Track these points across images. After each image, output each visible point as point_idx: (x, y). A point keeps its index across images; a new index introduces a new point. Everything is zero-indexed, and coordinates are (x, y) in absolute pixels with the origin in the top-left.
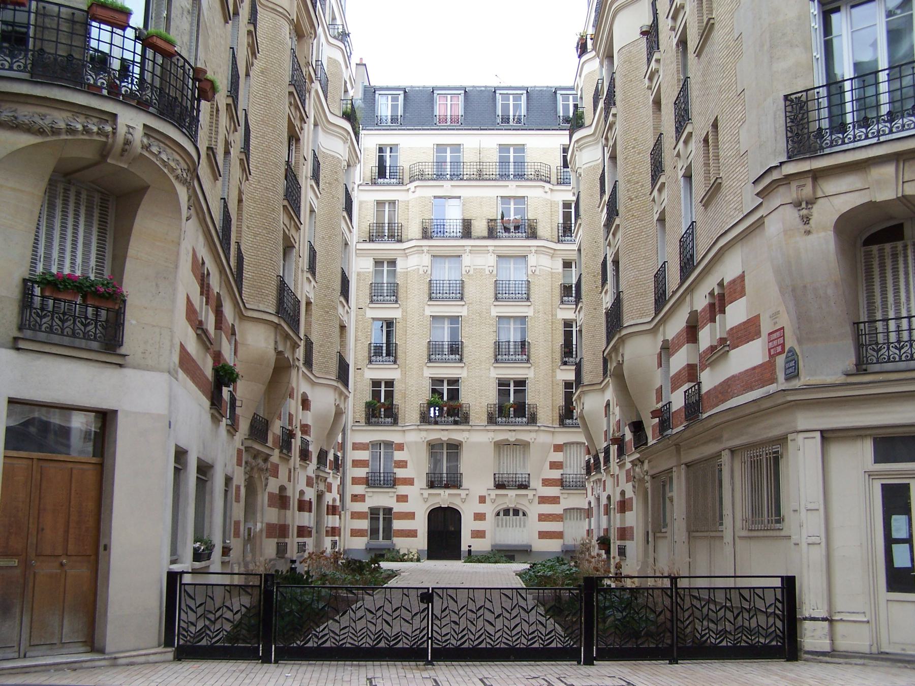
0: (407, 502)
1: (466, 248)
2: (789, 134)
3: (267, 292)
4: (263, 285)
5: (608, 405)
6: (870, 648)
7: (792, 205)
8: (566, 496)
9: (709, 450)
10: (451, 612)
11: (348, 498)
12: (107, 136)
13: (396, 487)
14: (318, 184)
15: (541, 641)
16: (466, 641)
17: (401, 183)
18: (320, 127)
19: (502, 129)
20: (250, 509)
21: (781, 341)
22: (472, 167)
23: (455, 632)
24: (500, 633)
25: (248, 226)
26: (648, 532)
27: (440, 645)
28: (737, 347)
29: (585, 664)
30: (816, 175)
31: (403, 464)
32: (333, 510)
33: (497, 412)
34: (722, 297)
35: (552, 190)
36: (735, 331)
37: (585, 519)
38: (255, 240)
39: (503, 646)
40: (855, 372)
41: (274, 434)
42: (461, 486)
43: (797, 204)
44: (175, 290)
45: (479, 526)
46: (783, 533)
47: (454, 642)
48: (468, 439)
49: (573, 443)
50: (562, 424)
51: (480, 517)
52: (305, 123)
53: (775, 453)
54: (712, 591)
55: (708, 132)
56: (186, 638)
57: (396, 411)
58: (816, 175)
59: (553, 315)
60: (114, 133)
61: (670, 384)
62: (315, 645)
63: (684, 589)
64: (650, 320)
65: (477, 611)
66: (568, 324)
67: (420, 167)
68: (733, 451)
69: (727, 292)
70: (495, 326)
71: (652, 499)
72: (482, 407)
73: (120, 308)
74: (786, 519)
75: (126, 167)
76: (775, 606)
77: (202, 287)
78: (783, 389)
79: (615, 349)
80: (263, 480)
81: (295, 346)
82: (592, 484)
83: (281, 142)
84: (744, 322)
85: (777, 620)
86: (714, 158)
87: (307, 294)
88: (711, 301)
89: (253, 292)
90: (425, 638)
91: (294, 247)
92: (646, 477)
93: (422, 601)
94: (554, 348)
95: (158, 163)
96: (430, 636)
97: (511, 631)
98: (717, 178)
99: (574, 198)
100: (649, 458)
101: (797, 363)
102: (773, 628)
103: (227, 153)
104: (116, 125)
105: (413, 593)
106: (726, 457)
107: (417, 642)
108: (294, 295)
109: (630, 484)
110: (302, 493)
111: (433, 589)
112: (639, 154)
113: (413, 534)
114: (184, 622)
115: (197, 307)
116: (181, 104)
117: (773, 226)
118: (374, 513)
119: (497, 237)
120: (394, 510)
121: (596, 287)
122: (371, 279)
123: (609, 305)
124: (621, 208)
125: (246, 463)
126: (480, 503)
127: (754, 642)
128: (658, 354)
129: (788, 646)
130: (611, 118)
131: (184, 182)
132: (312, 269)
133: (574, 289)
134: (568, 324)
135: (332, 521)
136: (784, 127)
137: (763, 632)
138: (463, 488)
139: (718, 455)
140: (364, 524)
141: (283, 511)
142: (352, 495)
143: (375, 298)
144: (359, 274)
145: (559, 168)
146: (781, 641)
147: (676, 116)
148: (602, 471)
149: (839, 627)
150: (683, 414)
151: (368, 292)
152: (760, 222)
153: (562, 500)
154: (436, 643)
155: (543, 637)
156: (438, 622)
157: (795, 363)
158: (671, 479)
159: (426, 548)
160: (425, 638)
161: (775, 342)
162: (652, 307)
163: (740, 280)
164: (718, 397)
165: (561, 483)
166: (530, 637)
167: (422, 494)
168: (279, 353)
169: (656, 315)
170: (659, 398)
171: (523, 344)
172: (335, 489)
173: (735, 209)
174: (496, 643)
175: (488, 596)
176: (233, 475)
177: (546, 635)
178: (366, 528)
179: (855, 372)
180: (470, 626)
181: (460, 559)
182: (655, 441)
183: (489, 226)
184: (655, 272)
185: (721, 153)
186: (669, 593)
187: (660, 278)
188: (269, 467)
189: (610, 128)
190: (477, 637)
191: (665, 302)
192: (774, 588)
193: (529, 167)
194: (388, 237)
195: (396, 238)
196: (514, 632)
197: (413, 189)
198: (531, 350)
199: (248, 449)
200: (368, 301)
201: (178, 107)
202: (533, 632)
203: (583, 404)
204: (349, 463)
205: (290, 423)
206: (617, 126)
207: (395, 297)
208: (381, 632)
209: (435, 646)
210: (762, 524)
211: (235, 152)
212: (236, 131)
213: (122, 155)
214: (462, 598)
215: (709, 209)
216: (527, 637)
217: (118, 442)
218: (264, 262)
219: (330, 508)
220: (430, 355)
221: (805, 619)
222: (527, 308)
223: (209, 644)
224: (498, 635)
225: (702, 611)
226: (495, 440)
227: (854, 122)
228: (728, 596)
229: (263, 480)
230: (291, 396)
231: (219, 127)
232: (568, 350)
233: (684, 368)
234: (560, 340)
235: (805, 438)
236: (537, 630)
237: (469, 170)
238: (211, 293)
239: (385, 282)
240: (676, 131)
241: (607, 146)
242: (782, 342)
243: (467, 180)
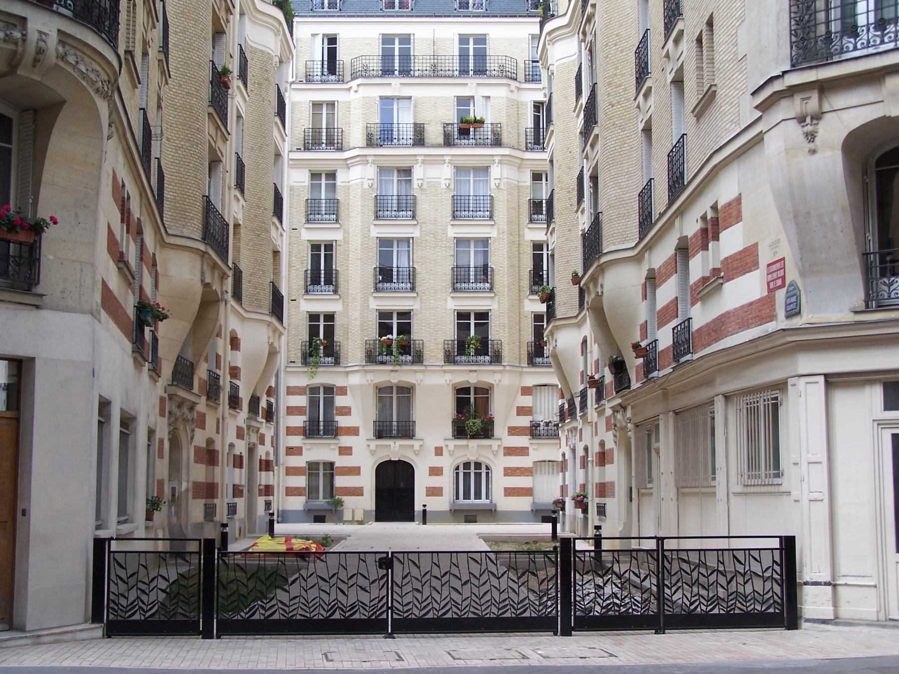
2: (794, 39)
3: (191, 215)
4: (187, 207)
5: (585, 342)
6: (878, 616)
7: (795, 121)
9: (701, 395)
10: (413, 579)
11: (282, 451)
12: (16, 44)
13: (339, 437)
14: (245, 84)
17: (341, 81)
18: (246, 17)
19: (460, 16)
20: (175, 466)
21: (781, 273)
22: (424, 61)
23: (418, 601)
25: (167, 138)
26: (631, 488)
27: (401, 615)
28: (733, 279)
29: (563, 634)
30: (824, 88)
31: (346, 411)
32: (267, 466)
33: (456, 350)
34: (716, 222)
35: (519, 89)
37: (558, 473)
38: (176, 155)
39: (471, 615)
40: (863, 308)
41: (200, 379)
42: (413, 435)
43: (801, 120)
44: (96, 220)
45: (435, 482)
46: (782, 489)
47: (416, 612)
50: (531, 363)
51: (436, 471)
52: (232, 14)
53: (773, 399)
55: (702, 31)
56: (117, 612)
57: (338, 348)
58: (824, 88)
60: (24, 41)
61: (656, 320)
62: (262, 617)
64: (633, 245)
65: (442, 577)
66: (538, 247)
67: (364, 61)
68: (727, 397)
69: (721, 216)
70: (452, 249)
71: (635, 451)
72: (437, 344)
73: (35, 241)
74: (785, 473)
75: (39, 79)
76: (773, 569)
77: (122, 214)
78: (783, 328)
79: (594, 279)
80: (189, 432)
81: (223, 277)
82: (566, 433)
83: (205, 39)
85: (775, 585)
86: (708, 61)
88: (703, 226)
89: (175, 215)
90: (384, 608)
92: (629, 425)
93: (381, 567)
94: (521, 274)
95: (75, 75)
96: (390, 605)
97: (480, 599)
98: (711, 85)
99: (546, 99)
100: (632, 404)
101: (798, 298)
102: (770, 594)
103: (145, 54)
104: (25, 30)
105: (370, 559)
106: (719, 403)
107: (376, 612)
108: (222, 217)
109: (611, 433)
110: (232, 446)
111: (392, 553)
112: (622, 52)
113: (358, 492)
114: (114, 593)
115: (118, 237)
116: (100, 6)
117: (774, 144)
118: (313, 466)
119: (454, 145)
120: (336, 465)
122: (306, 195)
123: (586, 227)
124: (601, 116)
125: (170, 413)
126: (436, 455)
127: (749, 609)
129: (787, 613)
130: (589, 9)
131: (106, 96)
132: (240, 185)
133: (544, 205)
134: (538, 247)
135: (264, 478)
136: (788, 31)
137: (760, 598)
139: (711, 402)
140: (301, 481)
141: (210, 467)
142: (287, 447)
143: (312, 216)
144: (292, 189)
145: (527, 62)
146: (780, 608)
147: (665, 9)
148: (578, 418)
149: (841, 589)
150: (671, 354)
151: (303, 209)
152: (759, 139)
154: (396, 613)
155: (516, 606)
157: (797, 299)
158: (657, 426)
159: (374, 508)
160: (384, 608)
161: (775, 275)
162: (635, 230)
165: (534, 431)
166: (501, 605)
167: (369, 446)
168: (206, 286)
169: (641, 239)
170: (644, 335)
171: (485, 267)
172: (268, 440)
173: (732, 121)
174: (463, 613)
175: (454, 561)
176: (156, 427)
177: (519, 604)
178: (304, 485)
179: (863, 308)
180: (435, 594)
181: (414, 521)
182: (639, 385)
184: (640, 191)
185: (716, 57)
186: (552, 556)
187: (645, 196)
188: (195, 417)
189: (589, 20)
190: (442, 606)
191: (652, 226)
192: (772, 549)
193: (492, 61)
194: (326, 145)
195: (336, 145)
197: (355, 88)
199: (171, 397)
200: (304, 220)
201: (96, 8)
202: (505, 600)
203: (556, 341)
204: (282, 411)
205: (218, 366)
206: (597, 18)
207: (335, 216)
209: (395, 616)
210: (759, 478)
211: (153, 52)
212: (155, 28)
213: (34, 66)
214: (426, 563)
215: (702, 120)
217: (36, 394)
218: (188, 181)
219: (263, 463)
221: (806, 583)
223: (143, 618)
224: (465, 603)
225: (691, 575)
226: (453, 382)
227: (868, 24)
228: (721, 559)
229: (189, 432)
230: (219, 335)
231: (137, 26)
232: (537, 277)
234: (528, 265)
235: (807, 383)
236: (509, 597)
237: (421, 65)
238: (131, 217)
239: (323, 197)
240: (665, 27)
241: (585, 42)
242: (782, 275)
243: (418, 77)
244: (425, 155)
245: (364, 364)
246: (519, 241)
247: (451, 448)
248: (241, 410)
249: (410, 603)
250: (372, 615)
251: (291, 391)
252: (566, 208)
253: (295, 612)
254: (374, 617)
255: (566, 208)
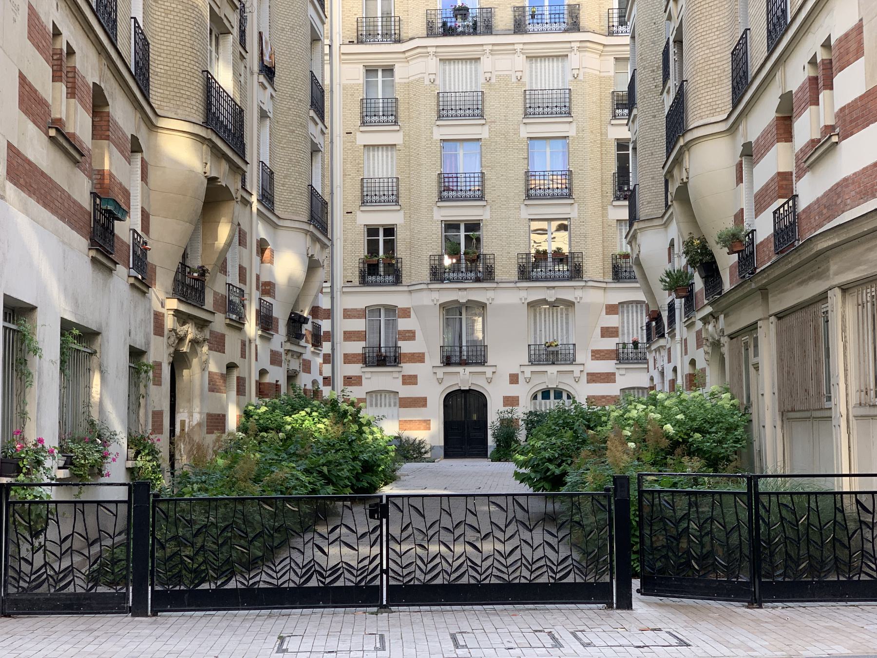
0: (416, 384)
1: (485, 47)
3: (188, 93)
4: (182, 83)
8: (623, 372)
10: (415, 531)
13: (402, 365)
15: (551, 574)
16: (438, 574)
24: (489, 562)
28: (852, 134)
31: (410, 335)
36: (847, 111)
38: (166, 19)
39: (494, 581)
42: (485, 362)
48: (493, 299)
49: (632, 302)
54: (813, 498)
59: (603, 134)
63: (769, 494)
64: (725, 116)
66: (622, 145)
72: (510, 258)
79: (678, 161)
84: (860, 97)
87: (262, 105)
88: (812, 74)
91: (230, 33)
93: (372, 517)
96: (385, 567)
97: (506, 559)
106: (835, 297)
107: (366, 577)
121: (656, 86)
128: (737, 165)
134: (622, 145)
138: (488, 364)
151: (358, 110)
153: (618, 377)
155: (554, 568)
156: (397, 548)
159: (442, 444)
160: (378, 571)
163: (855, 34)
164: (822, 214)
165: (618, 356)
166: (535, 567)
167: (435, 373)
174: (483, 577)
177: (559, 564)
183: (515, 16)
196: (510, 560)
198: (574, 181)
208: (312, 563)
209: (392, 582)
216: (530, 567)
220: (441, 192)
222: (567, 125)
233: (772, 179)
234: (613, 167)
238: (79, 82)
244: (493, 45)
245: (429, 282)
246: (602, 139)
247: (528, 374)
248: (277, 332)
249: (412, 563)
250: (361, 581)
251: (348, 314)
252: (650, 91)
253: (257, 579)
254: (363, 584)
255: (650, 91)
